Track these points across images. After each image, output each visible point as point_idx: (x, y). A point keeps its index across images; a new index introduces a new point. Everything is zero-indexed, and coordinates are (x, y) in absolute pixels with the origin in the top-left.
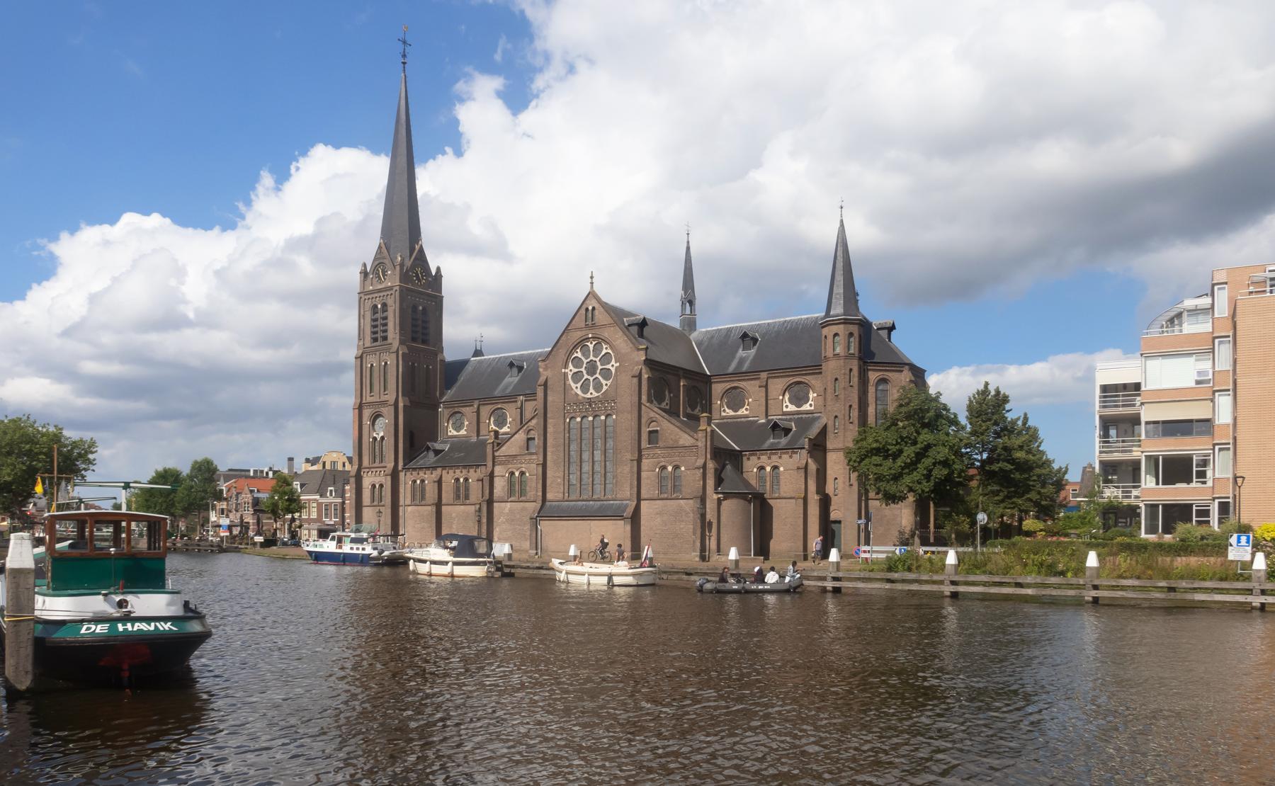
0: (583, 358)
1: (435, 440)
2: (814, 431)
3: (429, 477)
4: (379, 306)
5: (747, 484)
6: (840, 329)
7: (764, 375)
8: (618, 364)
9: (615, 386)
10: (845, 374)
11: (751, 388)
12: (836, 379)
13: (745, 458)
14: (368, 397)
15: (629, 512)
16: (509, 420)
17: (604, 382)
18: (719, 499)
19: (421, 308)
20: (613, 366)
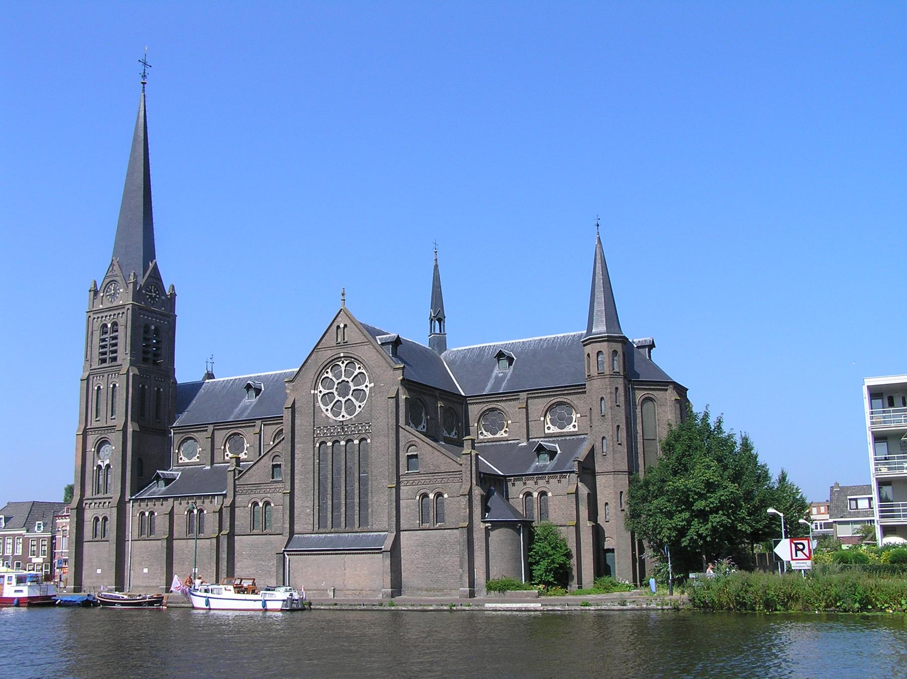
0: (334, 379)
1: (167, 467)
2: (582, 453)
3: (161, 510)
4: (109, 325)
5: (515, 512)
6: (604, 347)
7: (523, 396)
8: (372, 385)
9: (370, 407)
10: (611, 393)
11: (512, 409)
12: (602, 399)
13: (510, 484)
14: (93, 422)
15: (387, 545)
16: (246, 445)
17: (357, 404)
18: (486, 528)
19: (153, 327)
20: (366, 386)
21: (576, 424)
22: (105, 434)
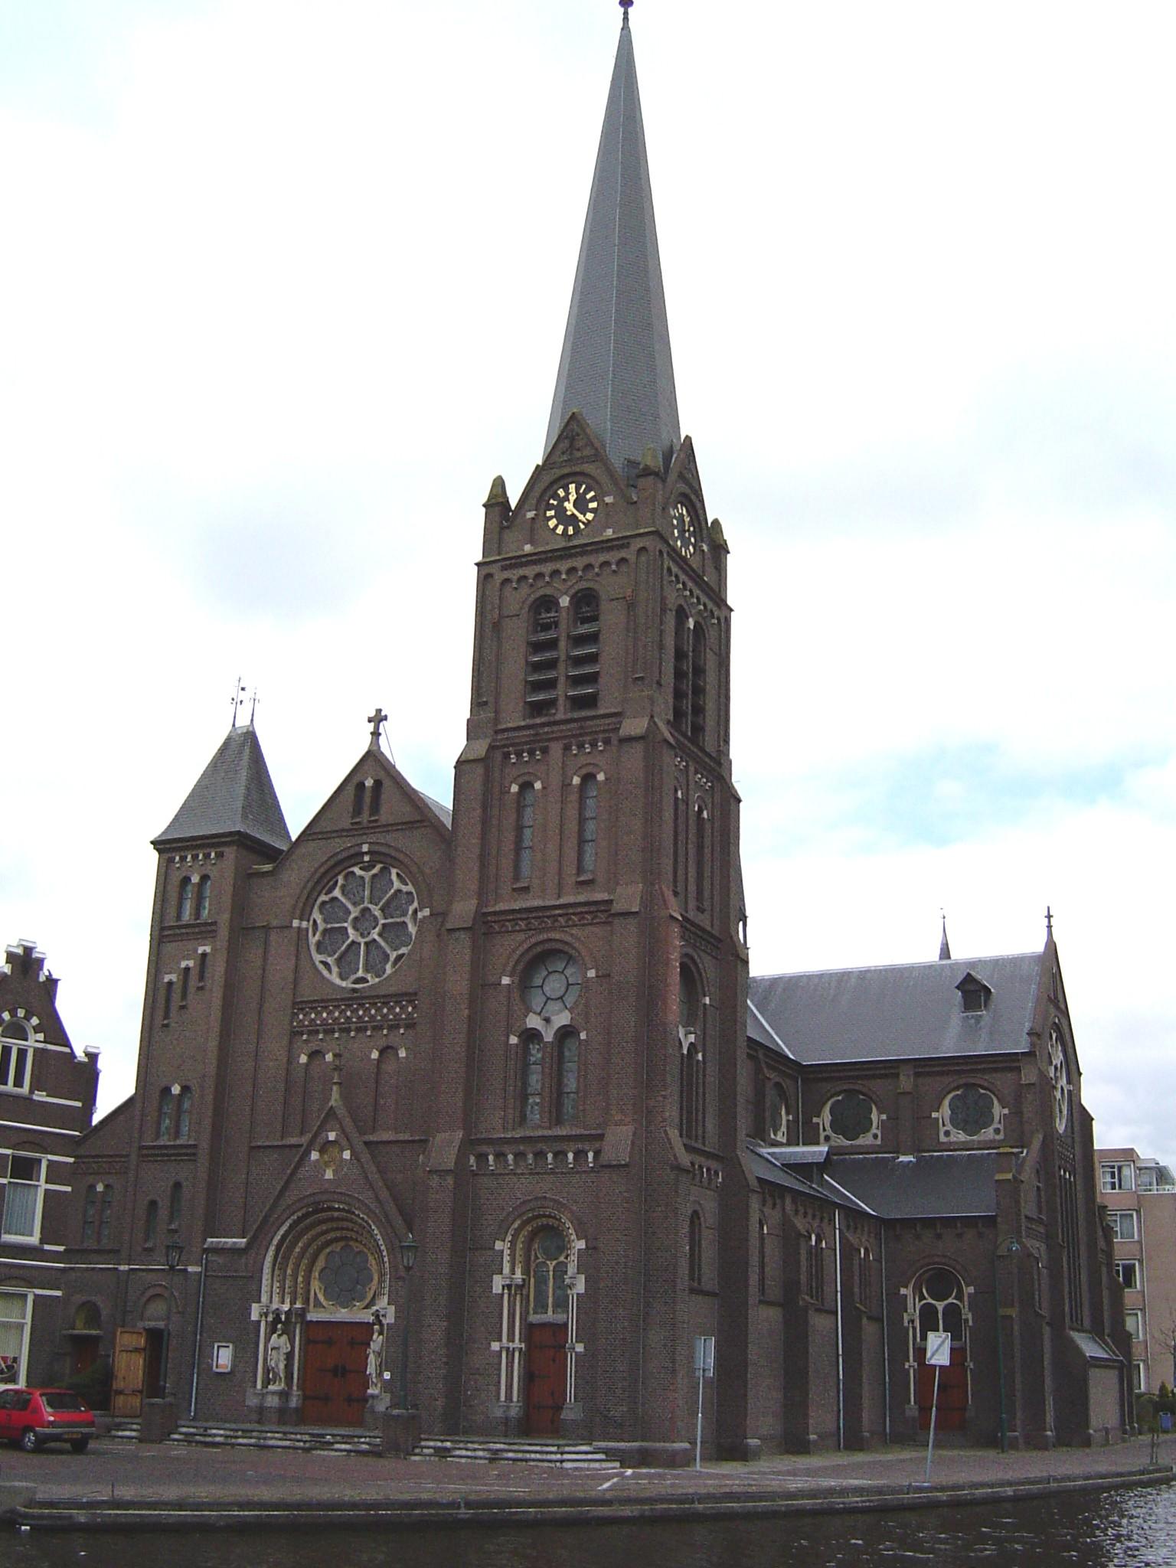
4: (565, 601)
21: (1001, 1127)
22: (553, 929)
